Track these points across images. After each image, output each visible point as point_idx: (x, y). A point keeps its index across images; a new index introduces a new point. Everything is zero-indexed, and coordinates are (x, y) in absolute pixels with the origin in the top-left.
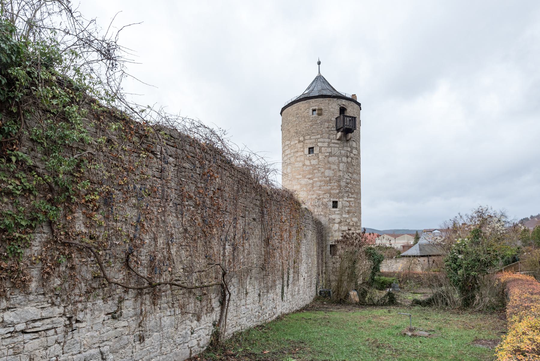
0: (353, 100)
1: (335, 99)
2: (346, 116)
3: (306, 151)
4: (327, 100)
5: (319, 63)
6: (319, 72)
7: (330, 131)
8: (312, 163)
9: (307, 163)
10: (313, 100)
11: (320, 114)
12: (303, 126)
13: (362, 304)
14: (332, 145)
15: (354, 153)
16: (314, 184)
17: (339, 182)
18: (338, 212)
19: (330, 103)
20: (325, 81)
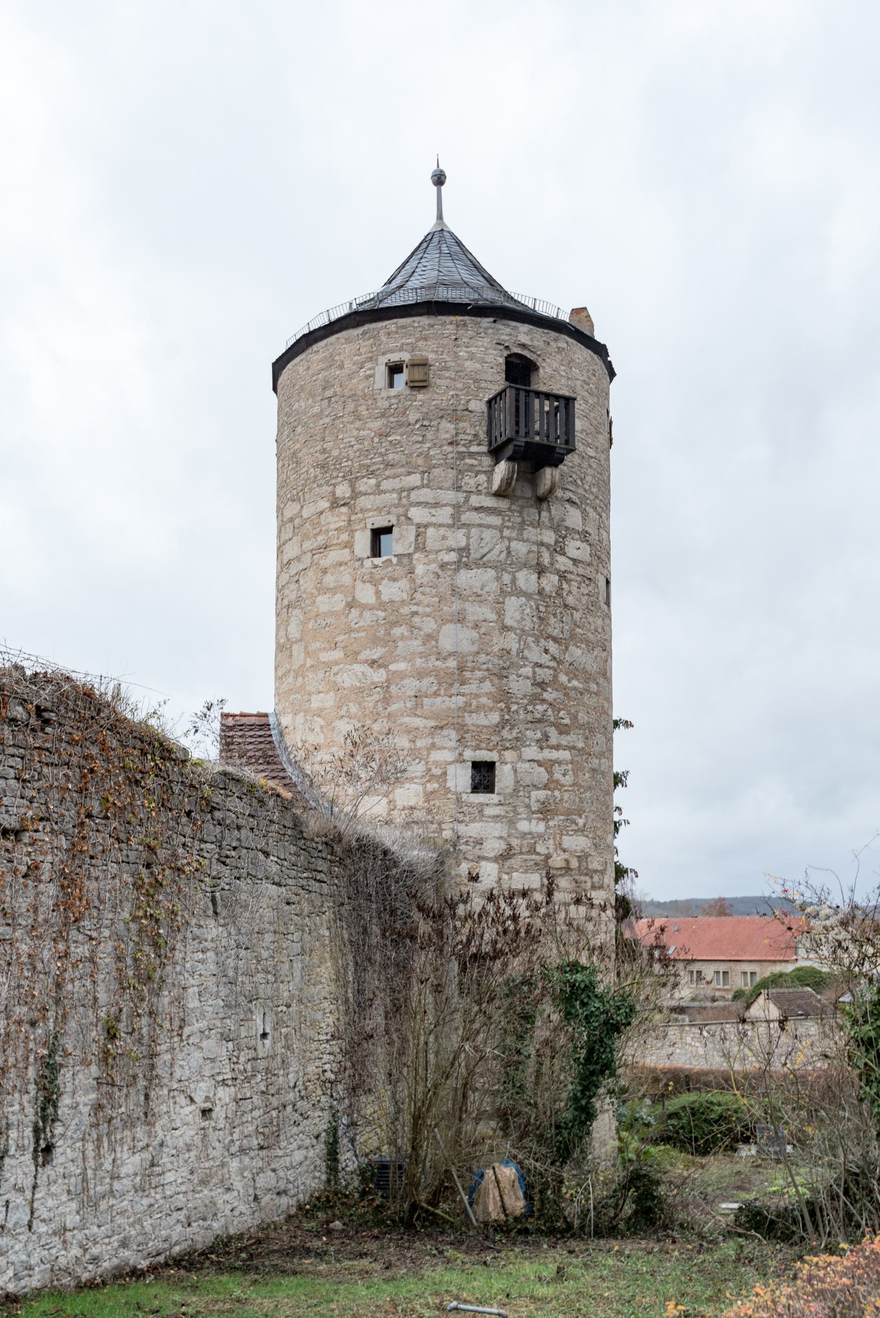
0: (577, 332)
1: (486, 322)
2: (538, 394)
3: (363, 541)
4: (448, 324)
5: (439, 179)
6: (440, 217)
7: (461, 456)
8: (385, 598)
9: (366, 594)
10: (391, 325)
11: (418, 386)
12: (349, 436)
13: (543, 1223)
14: (468, 517)
15: (572, 552)
16: (393, 689)
17: (501, 677)
18: (497, 811)
19: (465, 336)
20: (459, 251)
